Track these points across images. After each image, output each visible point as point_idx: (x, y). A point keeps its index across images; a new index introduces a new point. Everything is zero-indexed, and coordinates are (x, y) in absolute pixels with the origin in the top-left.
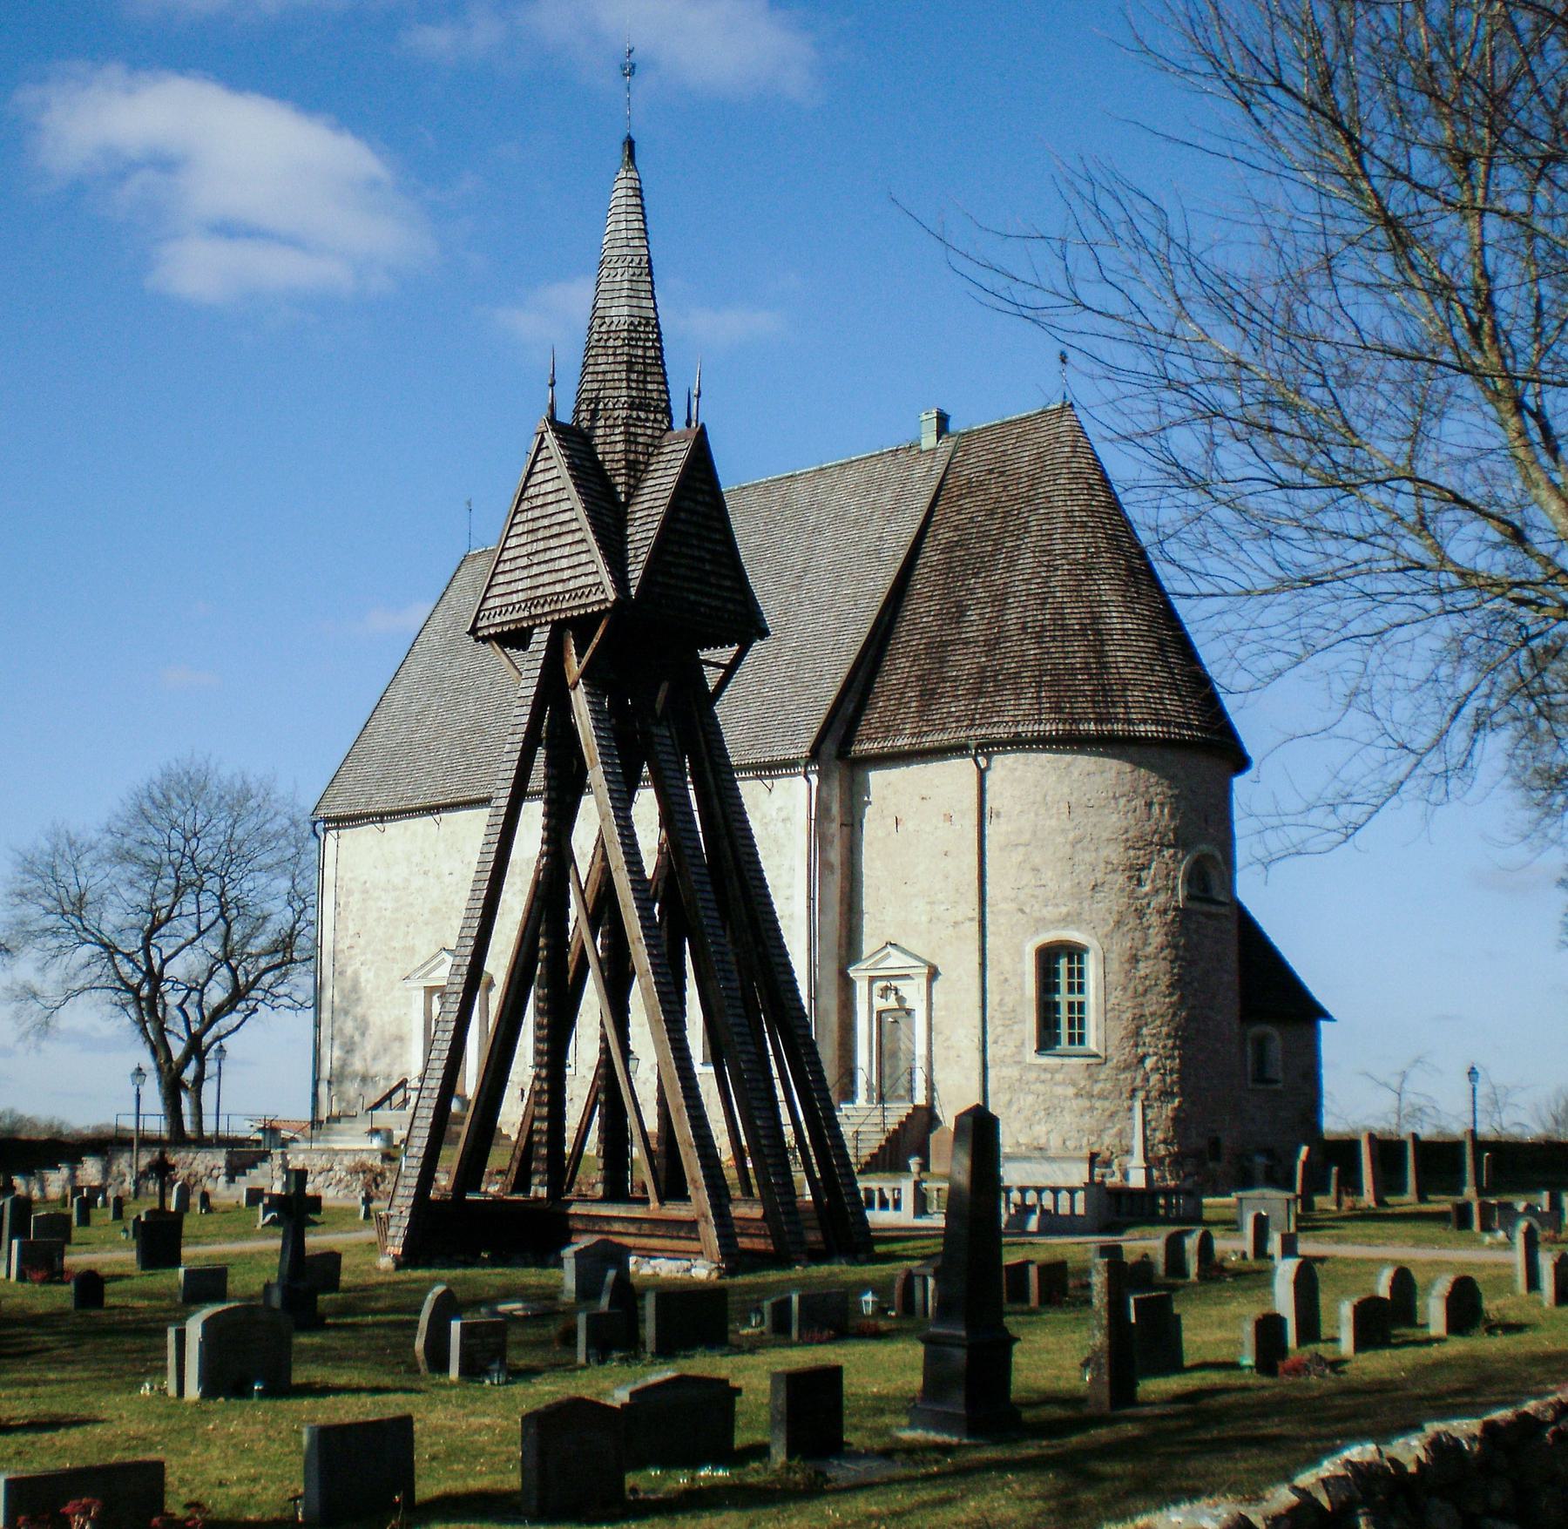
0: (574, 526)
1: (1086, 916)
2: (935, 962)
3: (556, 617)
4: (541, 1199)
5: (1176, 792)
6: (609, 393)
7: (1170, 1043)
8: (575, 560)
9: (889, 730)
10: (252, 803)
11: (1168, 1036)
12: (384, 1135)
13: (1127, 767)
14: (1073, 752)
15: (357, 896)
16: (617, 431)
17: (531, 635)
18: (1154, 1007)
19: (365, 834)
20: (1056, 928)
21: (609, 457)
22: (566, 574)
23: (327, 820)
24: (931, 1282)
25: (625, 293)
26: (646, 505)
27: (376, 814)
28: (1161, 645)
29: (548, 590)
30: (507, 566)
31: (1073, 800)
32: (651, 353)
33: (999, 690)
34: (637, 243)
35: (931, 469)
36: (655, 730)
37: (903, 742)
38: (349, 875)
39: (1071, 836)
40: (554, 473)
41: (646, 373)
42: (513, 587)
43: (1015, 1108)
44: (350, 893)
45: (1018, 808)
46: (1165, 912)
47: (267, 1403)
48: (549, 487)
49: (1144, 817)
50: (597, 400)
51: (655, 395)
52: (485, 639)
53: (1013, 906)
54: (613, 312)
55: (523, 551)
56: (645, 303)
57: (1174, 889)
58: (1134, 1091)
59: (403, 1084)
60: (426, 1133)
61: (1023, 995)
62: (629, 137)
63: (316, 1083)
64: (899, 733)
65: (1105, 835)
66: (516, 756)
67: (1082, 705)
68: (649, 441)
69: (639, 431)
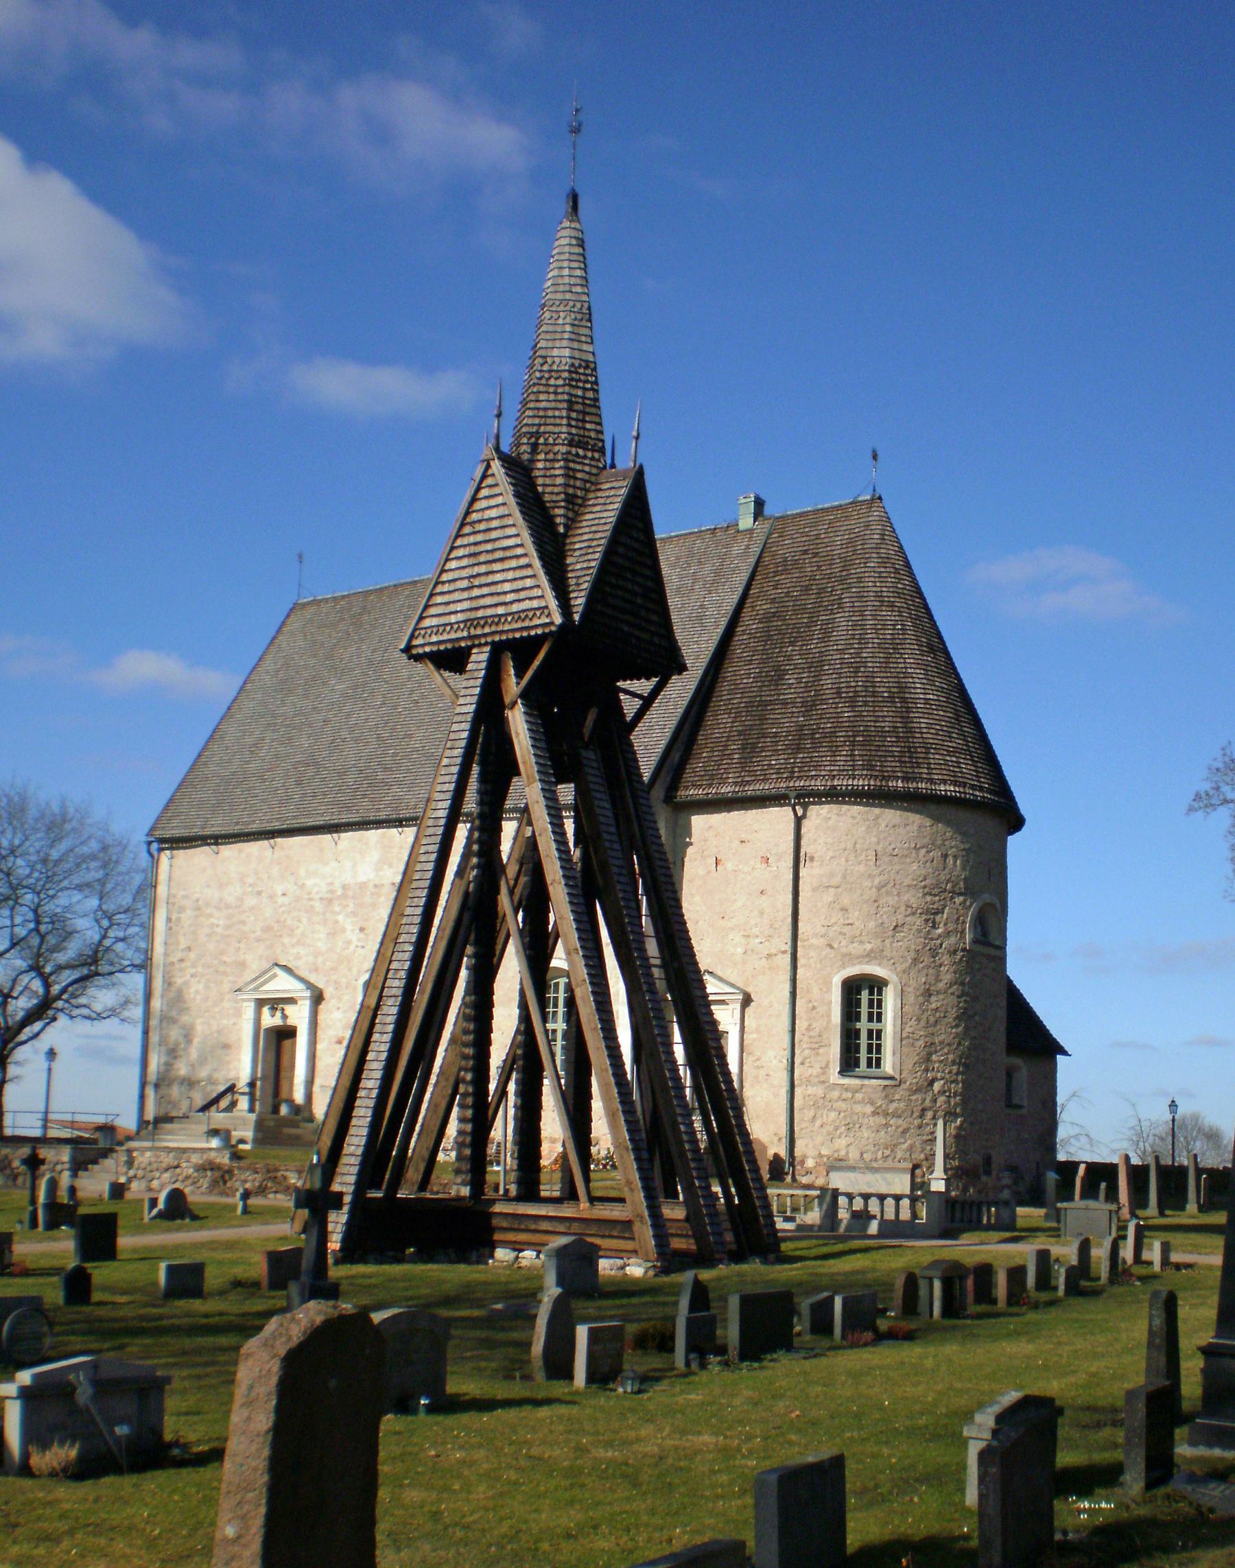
0: (519, 551)
1: (887, 953)
2: (749, 990)
3: (497, 638)
4: (464, 1198)
5: (967, 846)
6: (550, 428)
7: (955, 1068)
8: (519, 585)
9: (713, 778)
10: (68, 827)
11: (954, 1063)
12: (223, 1135)
13: (928, 822)
14: (882, 806)
15: (189, 913)
16: (557, 465)
17: (470, 654)
18: (943, 1037)
19: (200, 856)
20: (860, 963)
21: (549, 489)
22: (509, 598)
23: (162, 841)
24: (937, 1285)
25: (566, 336)
26: (586, 537)
27: (210, 837)
28: (957, 716)
29: (489, 612)
30: (446, 588)
31: (879, 848)
32: (590, 395)
33: (816, 745)
34: (579, 289)
35: (748, 547)
36: (583, 753)
37: (726, 790)
38: (183, 893)
39: (877, 881)
40: (500, 500)
41: (585, 413)
42: (452, 608)
43: (818, 1123)
44: (182, 909)
45: (830, 854)
46: (955, 952)
47: (432, 1419)
48: (493, 513)
49: (941, 866)
50: (537, 435)
51: (593, 435)
52: (418, 658)
53: (822, 942)
54: (555, 352)
55: (464, 573)
56: (585, 347)
57: (963, 932)
58: (923, 1110)
59: (231, 1089)
60: (365, 1132)
61: (830, 1020)
62: (573, 190)
63: (143, 1084)
64: (723, 782)
65: (907, 882)
66: (455, 769)
67: (892, 764)
68: (587, 477)
69: (578, 467)
